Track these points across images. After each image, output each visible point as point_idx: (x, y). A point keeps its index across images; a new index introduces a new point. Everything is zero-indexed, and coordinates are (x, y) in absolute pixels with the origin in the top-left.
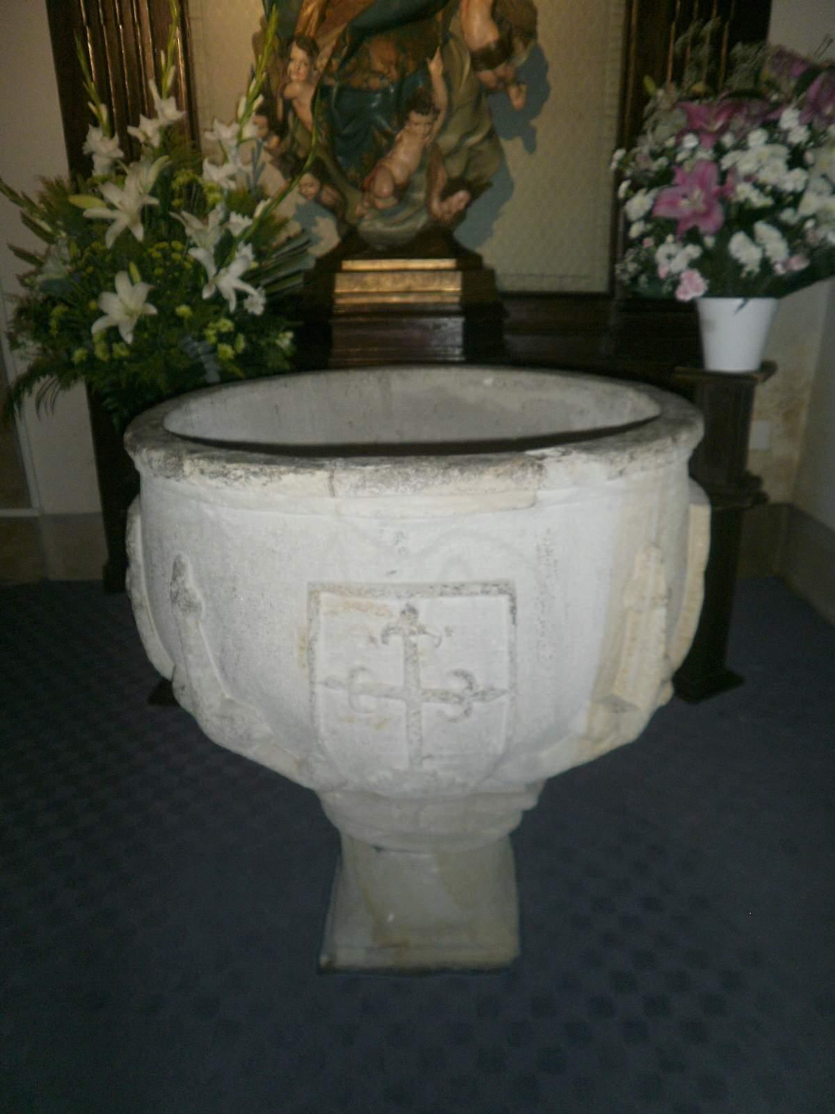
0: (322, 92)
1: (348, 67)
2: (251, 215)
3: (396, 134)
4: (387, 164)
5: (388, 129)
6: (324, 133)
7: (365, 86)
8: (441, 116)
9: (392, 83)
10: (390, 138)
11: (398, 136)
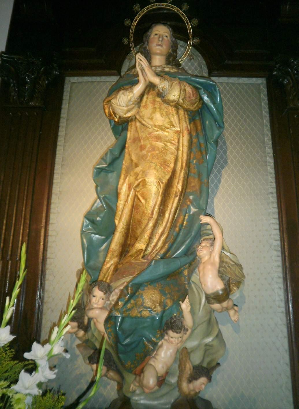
0: (110, 320)
1: (129, 306)
2: (78, 356)
3: (158, 342)
4: (152, 362)
5: (154, 339)
6: (111, 338)
7: (139, 315)
8: (188, 333)
9: (157, 314)
10: (155, 344)
11: (160, 343)
